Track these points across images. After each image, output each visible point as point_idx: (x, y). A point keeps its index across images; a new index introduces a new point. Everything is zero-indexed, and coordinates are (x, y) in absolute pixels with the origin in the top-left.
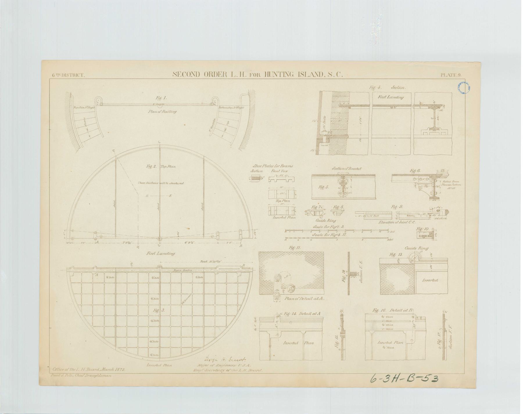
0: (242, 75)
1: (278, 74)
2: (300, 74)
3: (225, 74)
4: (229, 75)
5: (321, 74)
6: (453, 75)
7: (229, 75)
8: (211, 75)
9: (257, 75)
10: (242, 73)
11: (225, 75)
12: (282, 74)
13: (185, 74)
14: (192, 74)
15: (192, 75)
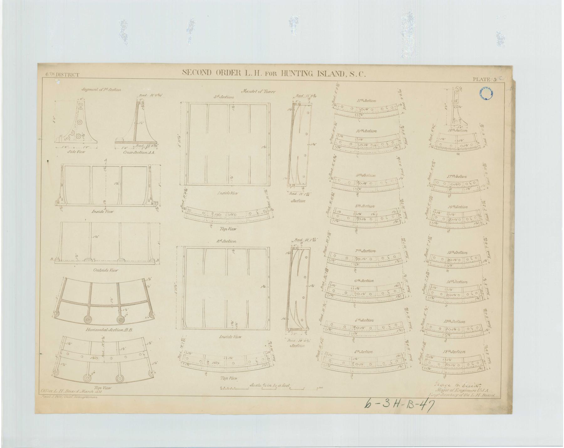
0: (257, 74)
1: (296, 73)
2: (320, 73)
3: (238, 73)
4: (243, 73)
5: (209, 72)
6: (486, 80)
7: (243, 73)
8: (223, 74)
9: (274, 74)
10: (257, 72)
11: (238, 74)
12: (300, 74)
13: (195, 72)
14: (304, 73)
15: (203, 73)
